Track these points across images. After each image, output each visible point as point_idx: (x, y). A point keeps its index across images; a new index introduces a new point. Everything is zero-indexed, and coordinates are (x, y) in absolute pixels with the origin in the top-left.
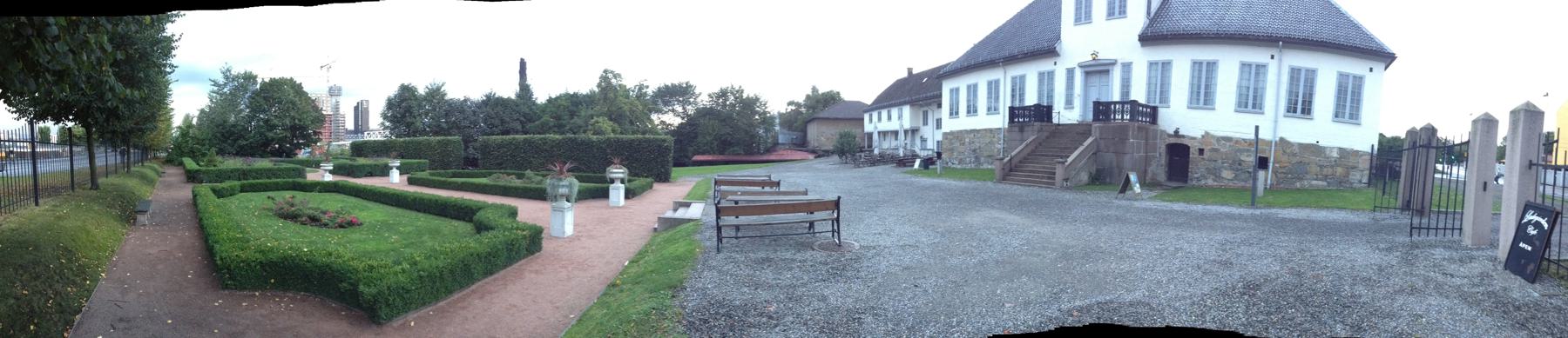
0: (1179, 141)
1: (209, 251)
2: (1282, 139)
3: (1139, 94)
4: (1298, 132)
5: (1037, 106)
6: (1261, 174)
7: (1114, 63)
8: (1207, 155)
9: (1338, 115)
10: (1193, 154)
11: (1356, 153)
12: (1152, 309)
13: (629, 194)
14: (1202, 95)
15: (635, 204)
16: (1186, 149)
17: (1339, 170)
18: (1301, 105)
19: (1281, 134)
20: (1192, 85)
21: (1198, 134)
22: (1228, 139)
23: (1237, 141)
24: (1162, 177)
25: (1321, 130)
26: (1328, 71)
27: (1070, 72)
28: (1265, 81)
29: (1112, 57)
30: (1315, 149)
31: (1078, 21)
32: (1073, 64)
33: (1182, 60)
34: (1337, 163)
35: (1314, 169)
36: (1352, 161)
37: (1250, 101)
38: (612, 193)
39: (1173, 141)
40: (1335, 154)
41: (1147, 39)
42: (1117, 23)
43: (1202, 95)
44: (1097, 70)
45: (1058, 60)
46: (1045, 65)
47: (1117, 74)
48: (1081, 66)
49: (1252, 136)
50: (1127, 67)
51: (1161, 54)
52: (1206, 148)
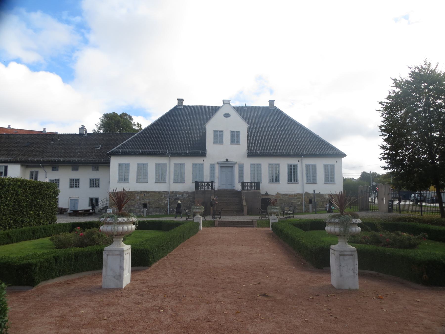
0: (266, 197)
1: (46, 175)
2: (306, 192)
3: (247, 178)
4: (310, 189)
6: (310, 205)
7: (235, 163)
13: (140, 260)
15: (162, 272)
18: (311, 177)
20: (288, 171)
21: (274, 194)
22: (286, 195)
23: (290, 195)
25: (322, 188)
27: (212, 166)
29: (235, 161)
32: (215, 161)
33: (265, 163)
38: (109, 261)
39: (264, 197)
41: (251, 155)
44: (227, 166)
46: (198, 160)
47: (237, 168)
48: (218, 163)
50: (241, 166)
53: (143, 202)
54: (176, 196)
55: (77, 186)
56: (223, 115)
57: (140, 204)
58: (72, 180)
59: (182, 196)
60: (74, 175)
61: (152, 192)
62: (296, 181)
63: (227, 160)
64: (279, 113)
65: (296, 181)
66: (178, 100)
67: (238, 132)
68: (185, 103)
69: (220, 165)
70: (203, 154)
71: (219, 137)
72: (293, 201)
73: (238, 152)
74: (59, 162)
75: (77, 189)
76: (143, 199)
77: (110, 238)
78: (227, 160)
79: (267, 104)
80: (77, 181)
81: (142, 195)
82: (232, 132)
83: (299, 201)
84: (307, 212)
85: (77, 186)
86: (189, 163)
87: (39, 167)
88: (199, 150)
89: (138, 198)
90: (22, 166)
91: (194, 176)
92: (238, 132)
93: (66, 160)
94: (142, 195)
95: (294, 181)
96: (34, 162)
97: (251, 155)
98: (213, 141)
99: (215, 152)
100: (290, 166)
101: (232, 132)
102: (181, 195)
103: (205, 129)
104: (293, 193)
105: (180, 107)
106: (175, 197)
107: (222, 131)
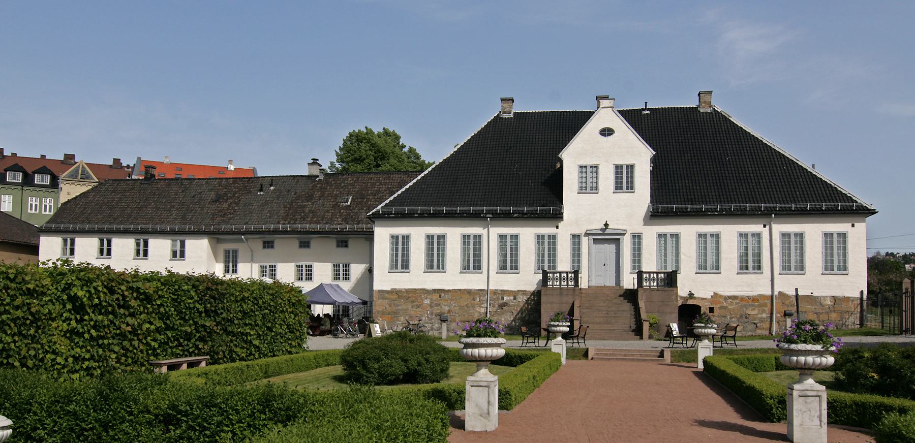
0: (690, 302)
4: (787, 285)
11: (847, 299)
14: (709, 263)
16: (697, 308)
17: (834, 316)
20: (392, 255)
21: (708, 295)
22: (734, 298)
23: (742, 299)
24: (351, 307)
26: (814, 232)
27: (576, 238)
28: (739, 247)
31: (582, 190)
32: (581, 231)
33: (688, 232)
34: (833, 309)
36: (844, 307)
37: (472, 263)
40: (829, 302)
41: (656, 215)
42: (624, 197)
43: (709, 263)
44: (607, 237)
46: (546, 230)
49: (794, 293)
50: (637, 238)
52: (716, 307)
53: (437, 310)
54: (503, 298)
56: (598, 132)
57: (432, 314)
59: (515, 299)
61: (455, 291)
63: (606, 225)
64: (720, 121)
67: (631, 168)
69: (591, 237)
70: (557, 216)
71: (589, 172)
75: (620, 162)
76: (438, 305)
78: (606, 225)
79: (691, 102)
82: (618, 168)
83: (764, 311)
86: (527, 235)
89: (427, 302)
92: (631, 168)
97: (656, 215)
99: (579, 209)
101: (618, 168)
102: (512, 298)
104: (750, 294)
105: (506, 116)
106: (501, 302)
107: (596, 167)
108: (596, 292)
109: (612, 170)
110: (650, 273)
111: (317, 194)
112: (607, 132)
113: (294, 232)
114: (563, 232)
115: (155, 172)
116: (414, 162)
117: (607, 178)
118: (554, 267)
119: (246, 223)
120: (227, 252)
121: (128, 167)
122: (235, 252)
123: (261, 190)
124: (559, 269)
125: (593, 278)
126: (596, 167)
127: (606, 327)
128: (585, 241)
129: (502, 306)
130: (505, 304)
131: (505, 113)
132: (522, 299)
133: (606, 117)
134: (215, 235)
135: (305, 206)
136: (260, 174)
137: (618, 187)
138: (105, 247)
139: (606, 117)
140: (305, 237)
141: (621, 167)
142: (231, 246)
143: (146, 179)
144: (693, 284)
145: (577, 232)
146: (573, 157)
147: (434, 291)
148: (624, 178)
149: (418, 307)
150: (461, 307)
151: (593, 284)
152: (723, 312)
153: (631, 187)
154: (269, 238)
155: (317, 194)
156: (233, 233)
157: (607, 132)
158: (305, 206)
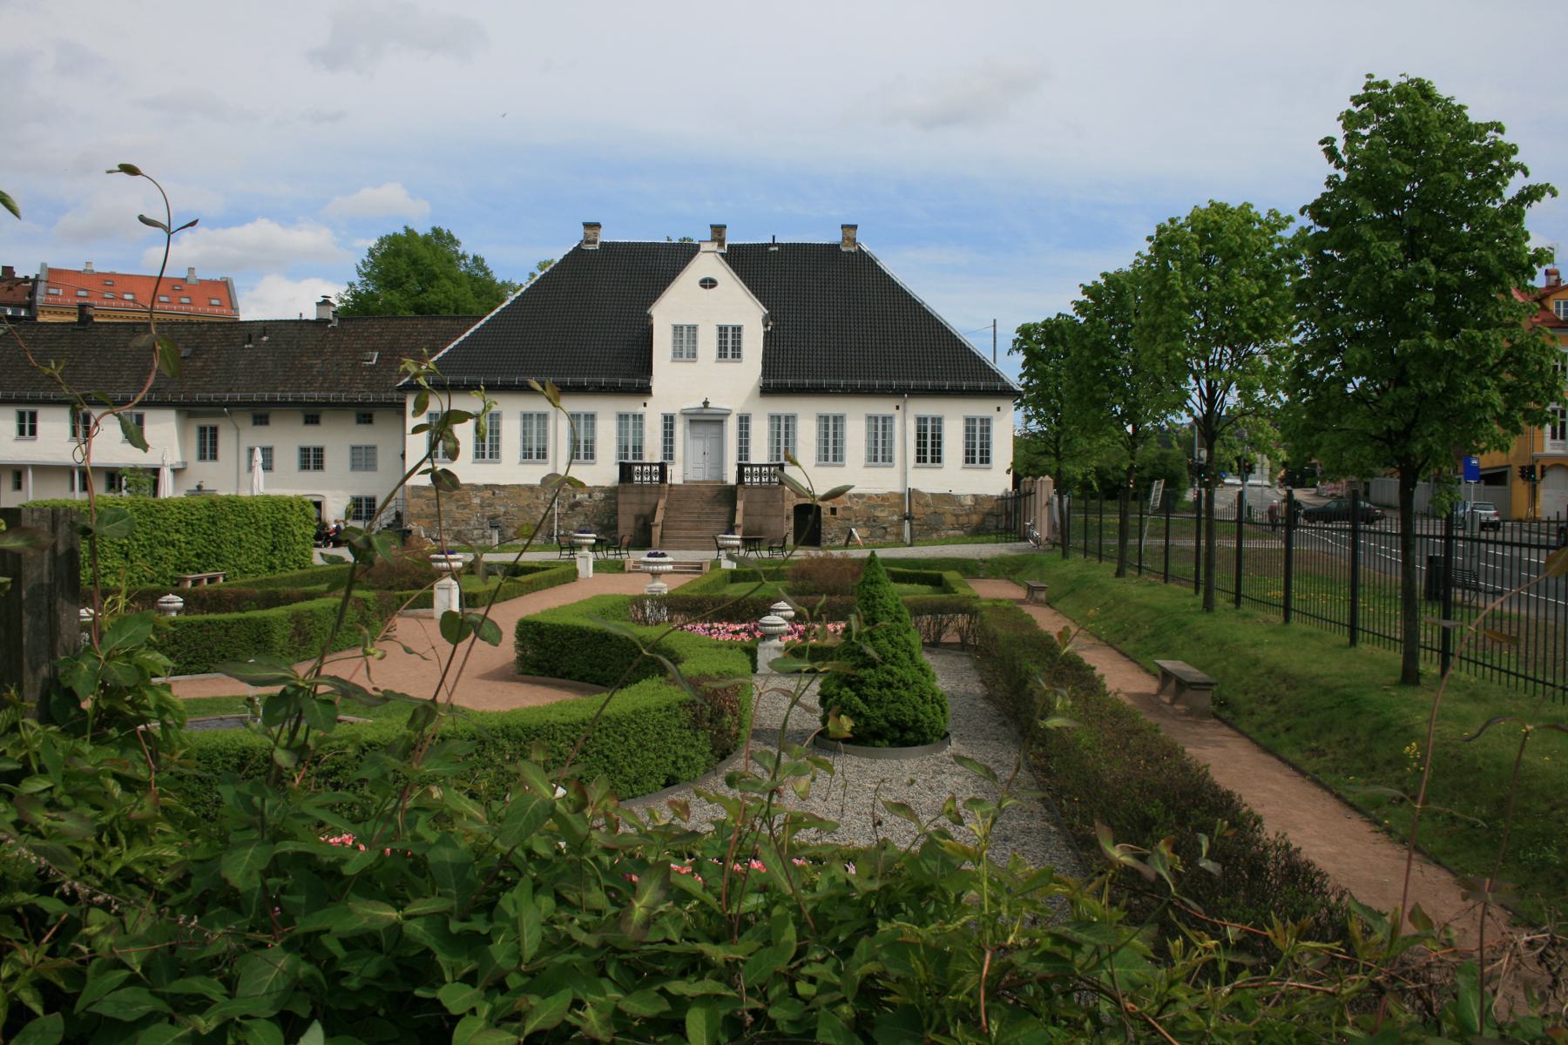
4: (929, 481)
5: (1419, 674)
8: (839, 513)
9: (969, 459)
10: (825, 514)
12: (641, 969)
14: (832, 451)
18: (929, 449)
19: (911, 485)
23: (870, 497)
26: (954, 418)
27: (669, 421)
30: (948, 498)
32: (674, 409)
33: (807, 415)
35: (949, 519)
37: (880, 452)
40: (969, 502)
41: (767, 390)
42: (729, 367)
43: (832, 451)
44: (706, 420)
45: (650, 401)
46: (630, 405)
47: (732, 426)
48: (684, 414)
50: (744, 421)
51: (783, 406)
53: (489, 512)
55: (319, 465)
58: (304, 451)
60: (312, 437)
61: (513, 486)
62: (888, 459)
63: (706, 403)
64: (865, 263)
65: (888, 459)
66: (587, 225)
67: (737, 330)
68: (605, 236)
70: (645, 391)
71: (685, 338)
72: (878, 513)
73: (735, 384)
74: (273, 403)
75: (318, 474)
76: (490, 505)
77: (439, 574)
78: (706, 403)
79: (834, 237)
80: (319, 452)
81: (488, 494)
82: (722, 330)
84: (900, 542)
85: (319, 465)
86: (606, 414)
87: (222, 415)
88: (632, 375)
89: (476, 501)
90: (179, 412)
91: (623, 449)
92: (737, 330)
93: (290, 396)
94: (488, 494)
95: (884, 459)
96: (210, 404)
97: (767, 390)
98: (670, 354)
99: (676, 384)
100: (873, 419)
101: (722, 330)
103: (650, 317)
104: (879, 491)
105: (590, 247)
107: (695, 328)
108: (689, 489)
109: (715, 333)
110: (760, 466)
111: (328, 349)
112: (709, 283)
113: (297, 403)
114: (653, 411)
115: (91, 312)
116: (485, 289)
117: (708, 343)
118: (641, 457)
119: (230, 390)
120: (202, 430)
121: (26, 279)
122: (214, 430)
123: (250, 342)
124: (647, 459)
125: (689, 470)
126: (695, 328)
127: (693, 533)
128: (680, 428)
129: (573, 506)
130: (578, 504)
131: (588, 242)
132: (598, 496)
133: (708, 263)
134: (187, 409)
135: (312, 366)
136: (250, 310)
137: (722, 354)
138: (27, 424)
139: (708, 263)
140: (312, 411)
141: (726, 329)
142: (208, 422)
143: (79, 323)
144: (812, 476)
145: (669, 411)
146: (666, 313)
147: (487, 487)
148: (730, 343)
149: (465, 507)
150: (521, 509)
151: (690, 477)
152: (847, 514)
153: (737, 355)
154: (261, 411)
155: (328, 349)
156: (210, 404)
157: (709, 283)
158: (312, 366)
